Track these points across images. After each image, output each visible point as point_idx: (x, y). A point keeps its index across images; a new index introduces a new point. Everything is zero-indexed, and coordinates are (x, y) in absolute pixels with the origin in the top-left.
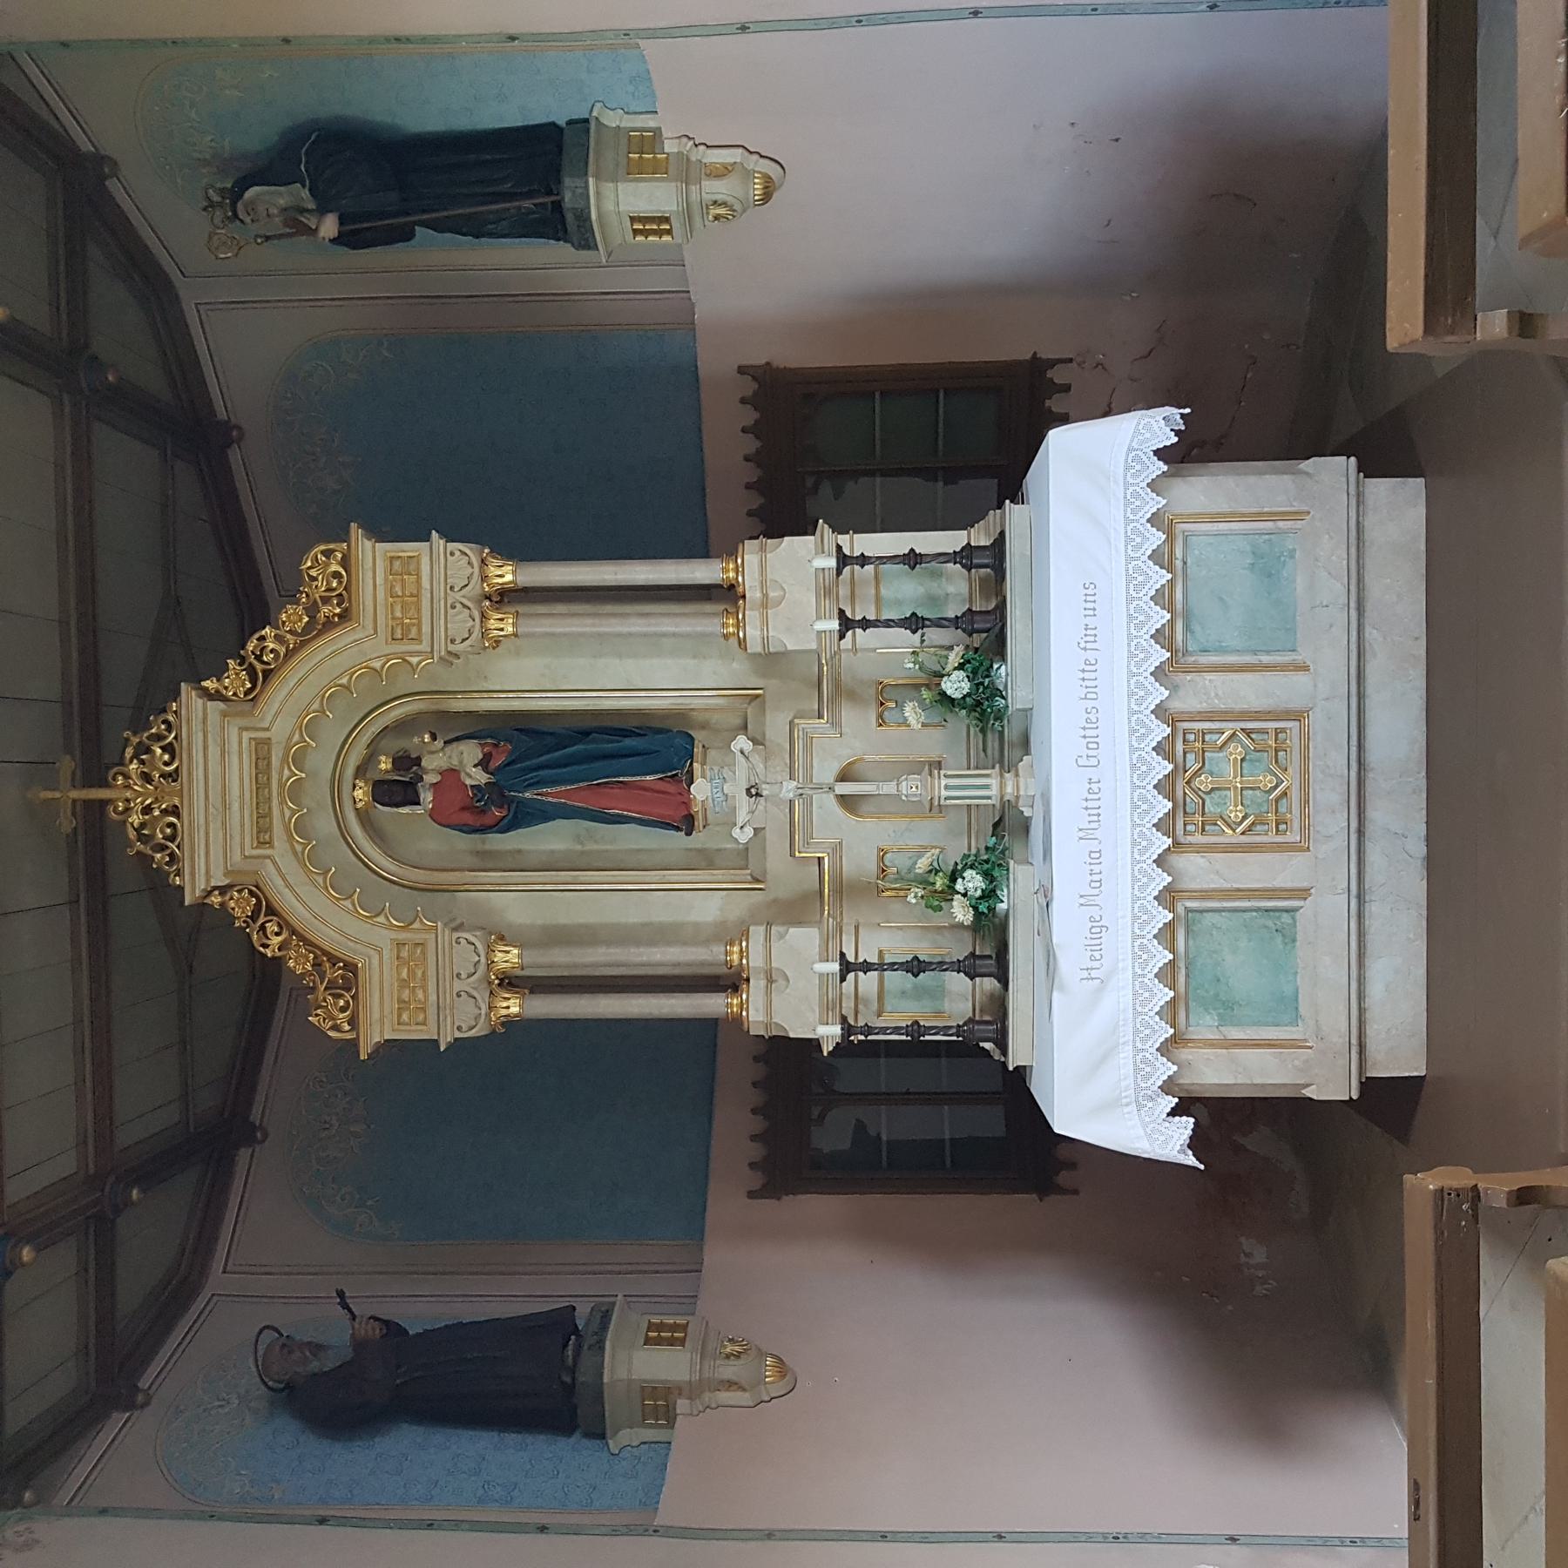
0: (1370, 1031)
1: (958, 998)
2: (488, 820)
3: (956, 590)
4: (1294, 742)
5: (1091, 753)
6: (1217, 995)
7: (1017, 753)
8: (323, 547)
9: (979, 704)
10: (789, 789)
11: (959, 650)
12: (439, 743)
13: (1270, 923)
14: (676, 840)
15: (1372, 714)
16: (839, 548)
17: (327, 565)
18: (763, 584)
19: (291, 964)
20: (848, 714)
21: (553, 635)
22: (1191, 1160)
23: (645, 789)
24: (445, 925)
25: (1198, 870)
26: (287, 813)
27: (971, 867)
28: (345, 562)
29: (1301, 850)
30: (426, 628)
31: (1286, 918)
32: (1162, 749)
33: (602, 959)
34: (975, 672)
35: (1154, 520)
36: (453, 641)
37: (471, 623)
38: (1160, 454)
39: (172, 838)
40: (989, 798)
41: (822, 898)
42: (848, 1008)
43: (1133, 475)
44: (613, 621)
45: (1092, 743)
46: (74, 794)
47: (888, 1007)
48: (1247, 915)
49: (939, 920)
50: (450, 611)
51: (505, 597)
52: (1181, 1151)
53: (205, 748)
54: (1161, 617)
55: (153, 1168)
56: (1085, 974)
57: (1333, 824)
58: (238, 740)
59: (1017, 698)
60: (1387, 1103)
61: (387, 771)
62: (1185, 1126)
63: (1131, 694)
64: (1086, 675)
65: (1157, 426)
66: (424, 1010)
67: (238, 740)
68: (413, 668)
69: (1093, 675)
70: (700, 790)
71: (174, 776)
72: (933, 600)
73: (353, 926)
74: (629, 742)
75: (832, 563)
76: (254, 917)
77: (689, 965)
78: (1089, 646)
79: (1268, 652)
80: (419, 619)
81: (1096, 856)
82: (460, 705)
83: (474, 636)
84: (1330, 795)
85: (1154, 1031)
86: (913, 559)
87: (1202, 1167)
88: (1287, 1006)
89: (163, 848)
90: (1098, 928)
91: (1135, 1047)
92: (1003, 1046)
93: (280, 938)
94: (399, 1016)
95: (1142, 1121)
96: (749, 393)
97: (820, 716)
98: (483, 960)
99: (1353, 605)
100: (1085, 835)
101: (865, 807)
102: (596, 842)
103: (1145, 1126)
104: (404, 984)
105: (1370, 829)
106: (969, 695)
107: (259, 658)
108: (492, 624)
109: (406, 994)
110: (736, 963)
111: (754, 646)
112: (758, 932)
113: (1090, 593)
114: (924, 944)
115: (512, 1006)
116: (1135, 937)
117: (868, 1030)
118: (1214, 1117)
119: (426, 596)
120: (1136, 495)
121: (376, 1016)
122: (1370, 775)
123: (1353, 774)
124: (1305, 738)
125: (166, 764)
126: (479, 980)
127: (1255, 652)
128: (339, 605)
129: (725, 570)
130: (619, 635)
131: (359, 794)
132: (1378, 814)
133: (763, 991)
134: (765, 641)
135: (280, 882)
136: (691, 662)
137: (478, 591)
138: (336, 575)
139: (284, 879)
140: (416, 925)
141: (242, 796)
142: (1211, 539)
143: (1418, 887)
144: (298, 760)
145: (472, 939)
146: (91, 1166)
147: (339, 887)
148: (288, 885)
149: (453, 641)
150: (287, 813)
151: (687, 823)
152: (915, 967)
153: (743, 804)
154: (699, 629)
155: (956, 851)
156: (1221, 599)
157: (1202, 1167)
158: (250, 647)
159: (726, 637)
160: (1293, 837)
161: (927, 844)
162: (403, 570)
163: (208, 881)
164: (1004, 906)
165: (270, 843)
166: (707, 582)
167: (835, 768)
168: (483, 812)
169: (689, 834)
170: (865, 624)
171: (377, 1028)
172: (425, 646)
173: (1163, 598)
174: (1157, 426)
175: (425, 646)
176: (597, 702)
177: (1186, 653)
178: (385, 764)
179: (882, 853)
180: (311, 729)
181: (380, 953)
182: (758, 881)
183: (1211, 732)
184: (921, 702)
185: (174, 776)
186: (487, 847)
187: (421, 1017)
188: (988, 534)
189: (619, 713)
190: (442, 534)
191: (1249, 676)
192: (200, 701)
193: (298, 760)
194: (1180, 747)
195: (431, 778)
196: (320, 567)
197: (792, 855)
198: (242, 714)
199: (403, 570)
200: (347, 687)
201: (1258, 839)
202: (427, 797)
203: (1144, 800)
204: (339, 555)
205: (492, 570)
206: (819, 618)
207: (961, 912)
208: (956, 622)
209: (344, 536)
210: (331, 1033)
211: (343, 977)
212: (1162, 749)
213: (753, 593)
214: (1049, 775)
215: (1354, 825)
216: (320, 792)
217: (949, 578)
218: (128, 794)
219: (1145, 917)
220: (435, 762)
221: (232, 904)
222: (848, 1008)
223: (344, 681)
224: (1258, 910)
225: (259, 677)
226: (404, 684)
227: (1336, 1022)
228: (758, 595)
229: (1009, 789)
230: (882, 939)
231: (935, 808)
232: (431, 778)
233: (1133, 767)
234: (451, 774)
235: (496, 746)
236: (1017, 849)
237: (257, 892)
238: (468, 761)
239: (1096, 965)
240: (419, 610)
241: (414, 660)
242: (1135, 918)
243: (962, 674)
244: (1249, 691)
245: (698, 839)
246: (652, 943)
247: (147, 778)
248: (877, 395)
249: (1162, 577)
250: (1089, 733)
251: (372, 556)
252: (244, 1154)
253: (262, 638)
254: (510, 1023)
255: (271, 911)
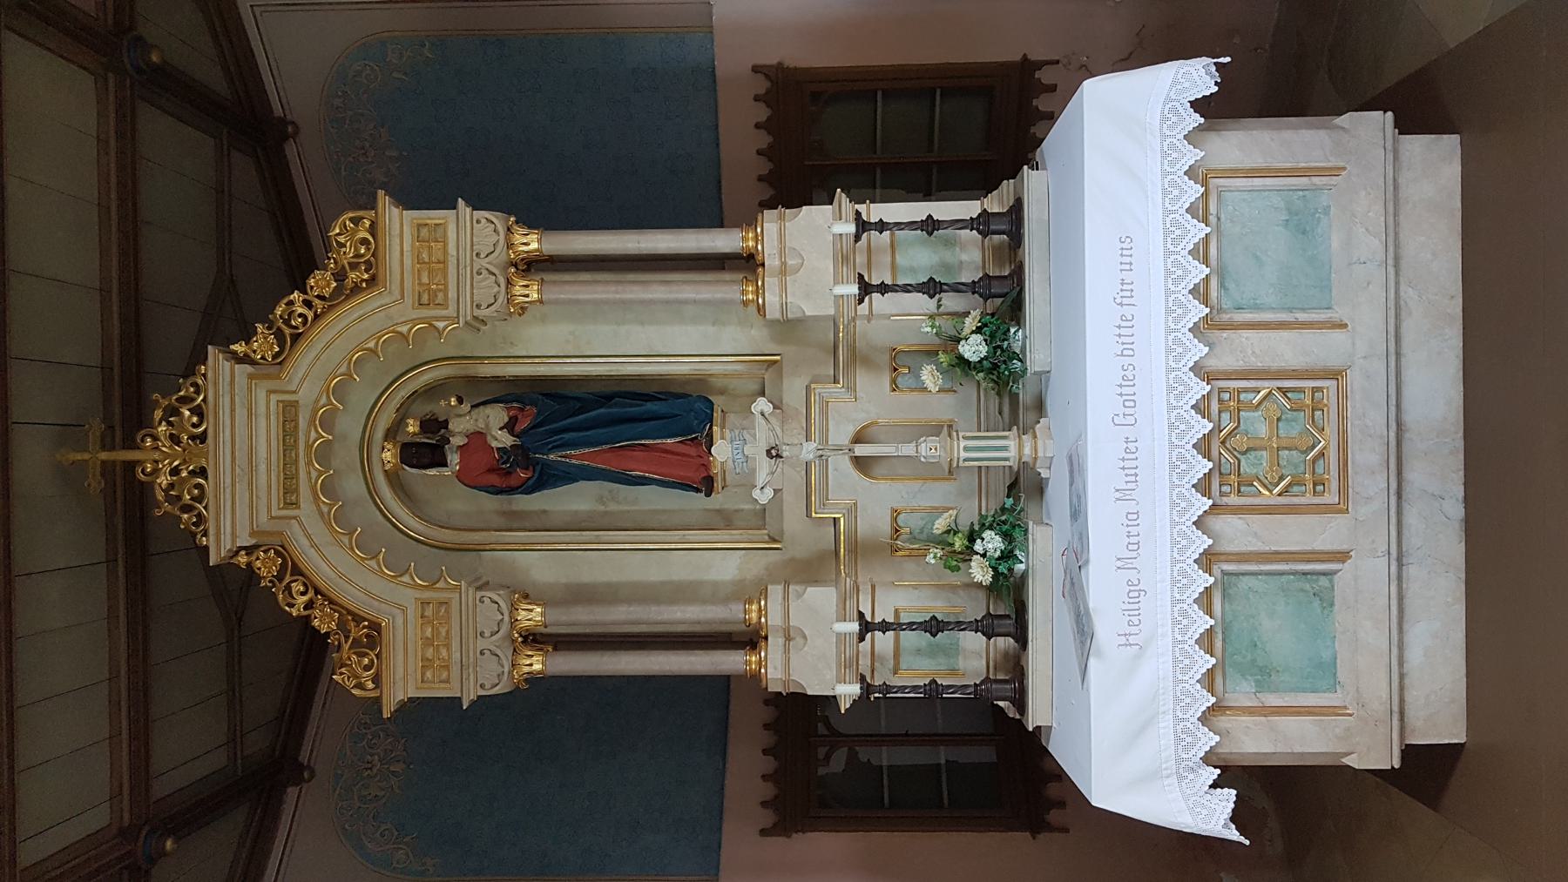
0: (1408, 698)
1: (972, 658)
2: (513, 482)
3: (969, 257)
4: (1330, 398)
5: (1128, 411)
6: (1254, 661)
7: (1031, 416)
8: (351, 215)
9: (995, 366)
10: (809, 450)
11: (976, 314)
12: (466, 407)
13: (1308, 587)
14: (695, 502)
15: (1409, 375)
16: (858, 214)
17: (355, 232)
18: (782, 252)
19: (316, 623)
20: (863, 379)
21: (578, 302)
22: (1233, 834)
23: (666, 451)
24: (469, 585)
25: (1238, 533)
26: (314, 474)
27: (991, 528)
28: (373, 229)
29: (1340, 512)
30: (452, 294)
31: (1323, 581)
32: (1201, 408)
33: (622, 617)
34: (992, 336)
35: (1191, 173)
36: (478, 306)
37: (496, 289)
38: (1197, 105)
39: (199, 499)
40: (1006, 459)
41: (836, 558)
42: (864, 665)
43: (1169, 127)
44: (635, 288)
45: (1129, 401)
46: (104, 456)
47: (903, 665)
48: (1284, 579)
49: (956, 579)
50: (477, 278)
51: (532, 266)
52: (1225, 826)
53: (233, 410)
54: (1199, 272)
55: (190, 815)
56: (1123, 640)
57: (1371, 485)
58: (265, 401)
59: (1036, 360)
60: (1425, 770)
61: (414, 434)
62: (1227, 798)
63: (1169, 351)
64: (1123, 331)
65: (1197, 76)
66: (447, 668)
67: (265, 401)
68: (440, 332)
69: (1129, 332)
70: (722, 451)
71: (203, 438)
72: (947, 267)
73: (378, 586)
74: (651, 406)
75: (851, 228)
76: (280, 578)
77: (708, 622)
78: (1125, 301)
79: (1303, 310)
80: (446, 285)
81: (1133, 518)
82: (487, 370)
83: (500, 300)
84: (1368, 456)
85: (1196, 700)
86: (930, 225)
87: (1247, 842)
88: (1325, 672)
89: (187, 509)
90: (1136, 592)
91: (1175, 716)
92: (1020, 702)
93: (305, 598)
94: (423, 674)
95: (1183, 793)
96: (762, 91)
97: (836, 381)
98: (506, 618)
99: (1391, 262)
100: (1123, 495)
101: (878, 470)
102: (618, 503)
103: (1186, 800)
104: (428, 642)
105: (1407, 489)
106: (986, 358)
107: (287, 322)
108: (518, 290)
109: (430, 653)
110: (755, 620)
111: (773, 312)
112: (775, 591)
113: (1126, 246)
114: (939, 604)
115: (535, 663)
116: (1175, 602)
117: (886, 688)
118: (1260, 787)
119: (452, 262)
120: (1172, 146)
121: (400, 672)
122: (1407, 435)
123: (1392, 435)
124: (1342, 396)
125: (194, 426)
126: (504, 638)
127: (1290, 310)
128: (367, 271)
129: (744, 239)
130: (642, 302)
131: (387, 455)
132: (1416, 475)
133: (781, 649)
134: (784, 307)
135: (305, 542)
136: (711, 329)
137: (504, 257)
138: (364, 241)
139: (309, 537)
140: (440, 585)
141: (269, 460)
142: (1246, 195)
143: (1456, 551)
144: (327, 423)
145: (496, 598)
146: (126, 816)
147: (366, 547)
148: (314, 545)
149: (478, 306)
150: (314, 474)
151: (707, 485)
152: (934, 626)
153: (764, 467)
154: (719, 296)
155: (969, 515)
156: (1257, 258)
157: (1247, 842)
158: (278, 312)
159: (745, 303)
160: (1331, 498)
161: (953, 506)
162: (429, 237)
163: (233, 541)
164: (1022, 567)
165: (296, 505)
166: (727, 250)
167: (850, 430)
168: (508, 473)
169: (708, 494)
170: (883, 289)
171: (400, 684)
172: (451, 311)
173: (1201, 253)
174: (1197, 76)
175: (451, 311)
176: (620, 367)
177: (1220, 311)
178: (412, 427)
179: (896, 513)
180: (339, 392)
181: (404, 612)
182: (774, 541)
183: (1246, 390)
184: (938, 365)
185: (203, 438)
186: (514, 508)
187: (445, 675)
188: (1001, 202)
189: (641, 379)
190: (468, 203)
191: (1285, 334)
192: (227, 365)
193: (327, 423)
194: (1215, 406)
195: (457, 441)
196: (346, 234)
197: (809, 515)
198: (268, 377)
199: (429, 237)
200: (373, 351)
201: (1296, 500)
202: (454, 459)
203: (1182, 458)
204: (367, 223)
205: (518, 238)
206: (836, 283)
207: (980, 572)
208: (973, 287)
209: (371, 204)
210: (354, 691)
211: (367, 636)
212: (1201, 408)
213: (772, 261)
214: (1081, 436)
215: (1394, 486)
216: (347, 455)
217: (963, 247)
218: (156, 456)
219: (1185, 581)
220: (461, 426)
221: (258, 564)
222: (864, 665)
223: (371, 345)
224: (1294, 573)
225: (289, 341)
226: (435, 349)
227: (1378, 689)
228: (777, 262)
229: (1027, 450)
230: (896, 599)
231: (952, 471)
232: (457, 441)
233: (1171, 426)
234: (478, 437)
235: (522, 410)
236: (1031, 509)
237: (282, 552)
238: (494, 423)
239: (1134, 630)
240: (445, 277)
241: (441, 325)
242: (1174, 582)
243: (979, 338)
244: (1286, 350)
245: (717, 500)
246: (672, 601)
247: (175, 440)
248: (879, 94)
249: (1199, 231)
250: (1125, 390)
251: (399, 224)
252: (292, 792)
253: (291, 303)
254: (533, 680)
255: (297, 571)
